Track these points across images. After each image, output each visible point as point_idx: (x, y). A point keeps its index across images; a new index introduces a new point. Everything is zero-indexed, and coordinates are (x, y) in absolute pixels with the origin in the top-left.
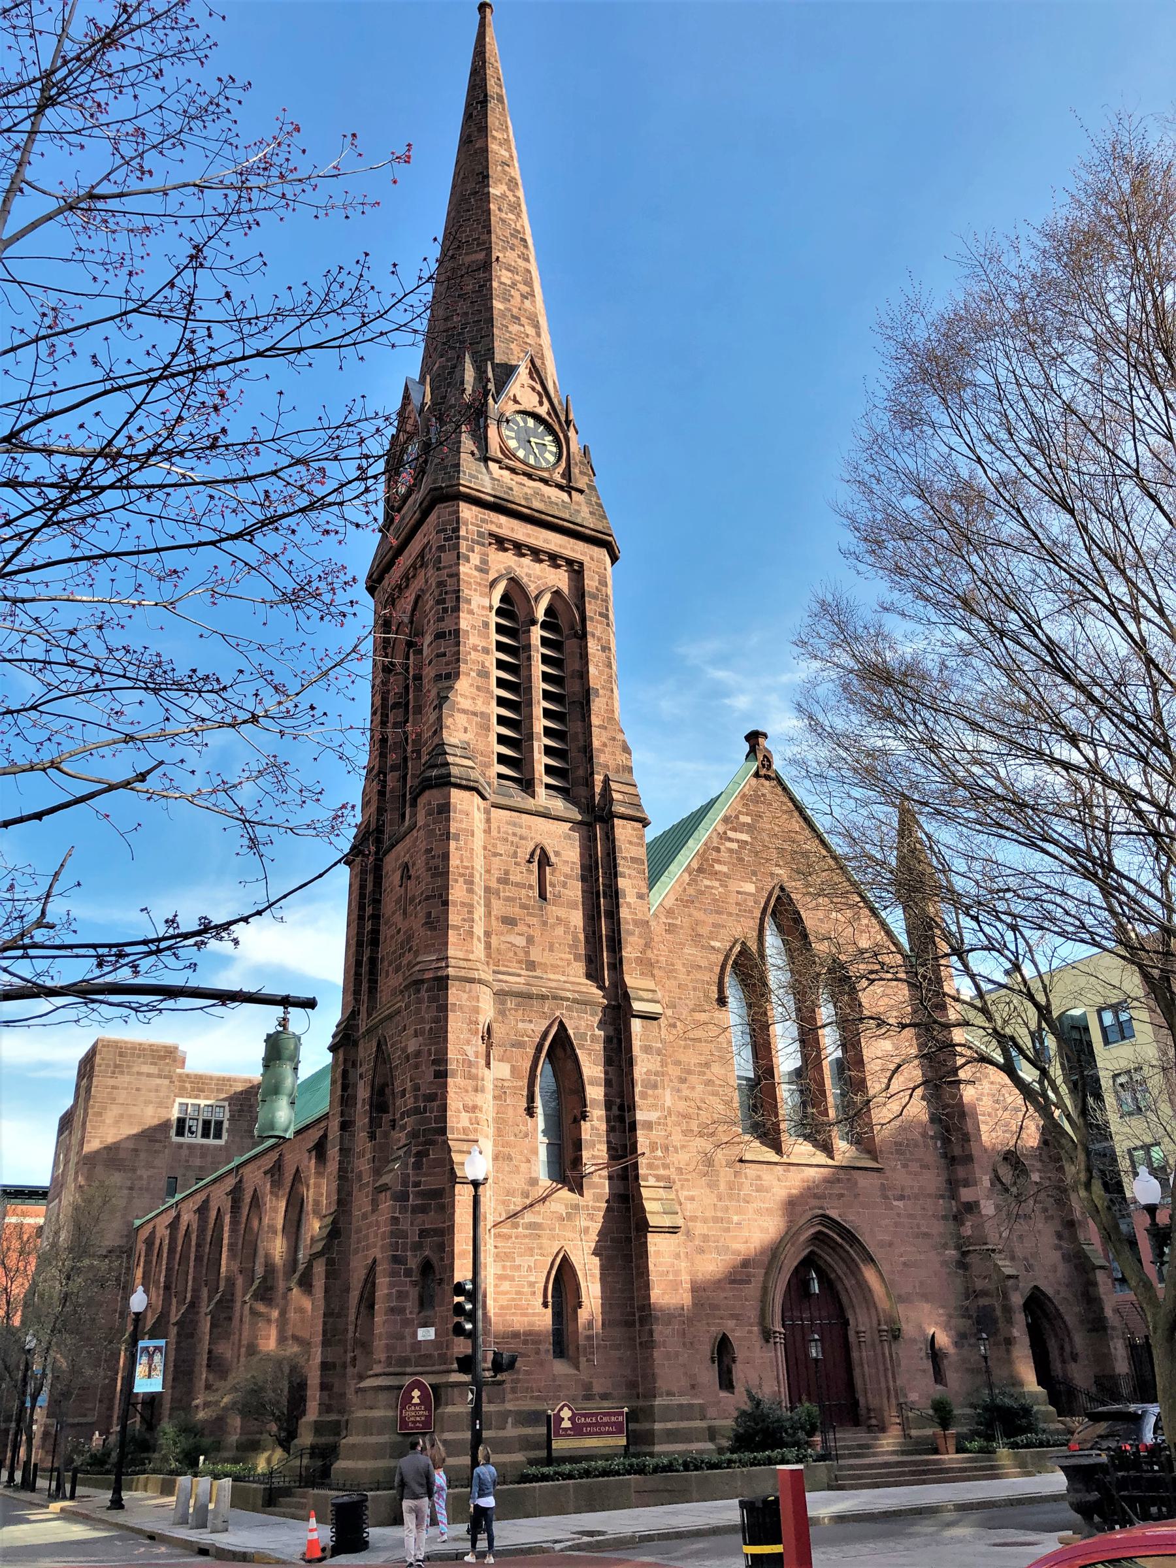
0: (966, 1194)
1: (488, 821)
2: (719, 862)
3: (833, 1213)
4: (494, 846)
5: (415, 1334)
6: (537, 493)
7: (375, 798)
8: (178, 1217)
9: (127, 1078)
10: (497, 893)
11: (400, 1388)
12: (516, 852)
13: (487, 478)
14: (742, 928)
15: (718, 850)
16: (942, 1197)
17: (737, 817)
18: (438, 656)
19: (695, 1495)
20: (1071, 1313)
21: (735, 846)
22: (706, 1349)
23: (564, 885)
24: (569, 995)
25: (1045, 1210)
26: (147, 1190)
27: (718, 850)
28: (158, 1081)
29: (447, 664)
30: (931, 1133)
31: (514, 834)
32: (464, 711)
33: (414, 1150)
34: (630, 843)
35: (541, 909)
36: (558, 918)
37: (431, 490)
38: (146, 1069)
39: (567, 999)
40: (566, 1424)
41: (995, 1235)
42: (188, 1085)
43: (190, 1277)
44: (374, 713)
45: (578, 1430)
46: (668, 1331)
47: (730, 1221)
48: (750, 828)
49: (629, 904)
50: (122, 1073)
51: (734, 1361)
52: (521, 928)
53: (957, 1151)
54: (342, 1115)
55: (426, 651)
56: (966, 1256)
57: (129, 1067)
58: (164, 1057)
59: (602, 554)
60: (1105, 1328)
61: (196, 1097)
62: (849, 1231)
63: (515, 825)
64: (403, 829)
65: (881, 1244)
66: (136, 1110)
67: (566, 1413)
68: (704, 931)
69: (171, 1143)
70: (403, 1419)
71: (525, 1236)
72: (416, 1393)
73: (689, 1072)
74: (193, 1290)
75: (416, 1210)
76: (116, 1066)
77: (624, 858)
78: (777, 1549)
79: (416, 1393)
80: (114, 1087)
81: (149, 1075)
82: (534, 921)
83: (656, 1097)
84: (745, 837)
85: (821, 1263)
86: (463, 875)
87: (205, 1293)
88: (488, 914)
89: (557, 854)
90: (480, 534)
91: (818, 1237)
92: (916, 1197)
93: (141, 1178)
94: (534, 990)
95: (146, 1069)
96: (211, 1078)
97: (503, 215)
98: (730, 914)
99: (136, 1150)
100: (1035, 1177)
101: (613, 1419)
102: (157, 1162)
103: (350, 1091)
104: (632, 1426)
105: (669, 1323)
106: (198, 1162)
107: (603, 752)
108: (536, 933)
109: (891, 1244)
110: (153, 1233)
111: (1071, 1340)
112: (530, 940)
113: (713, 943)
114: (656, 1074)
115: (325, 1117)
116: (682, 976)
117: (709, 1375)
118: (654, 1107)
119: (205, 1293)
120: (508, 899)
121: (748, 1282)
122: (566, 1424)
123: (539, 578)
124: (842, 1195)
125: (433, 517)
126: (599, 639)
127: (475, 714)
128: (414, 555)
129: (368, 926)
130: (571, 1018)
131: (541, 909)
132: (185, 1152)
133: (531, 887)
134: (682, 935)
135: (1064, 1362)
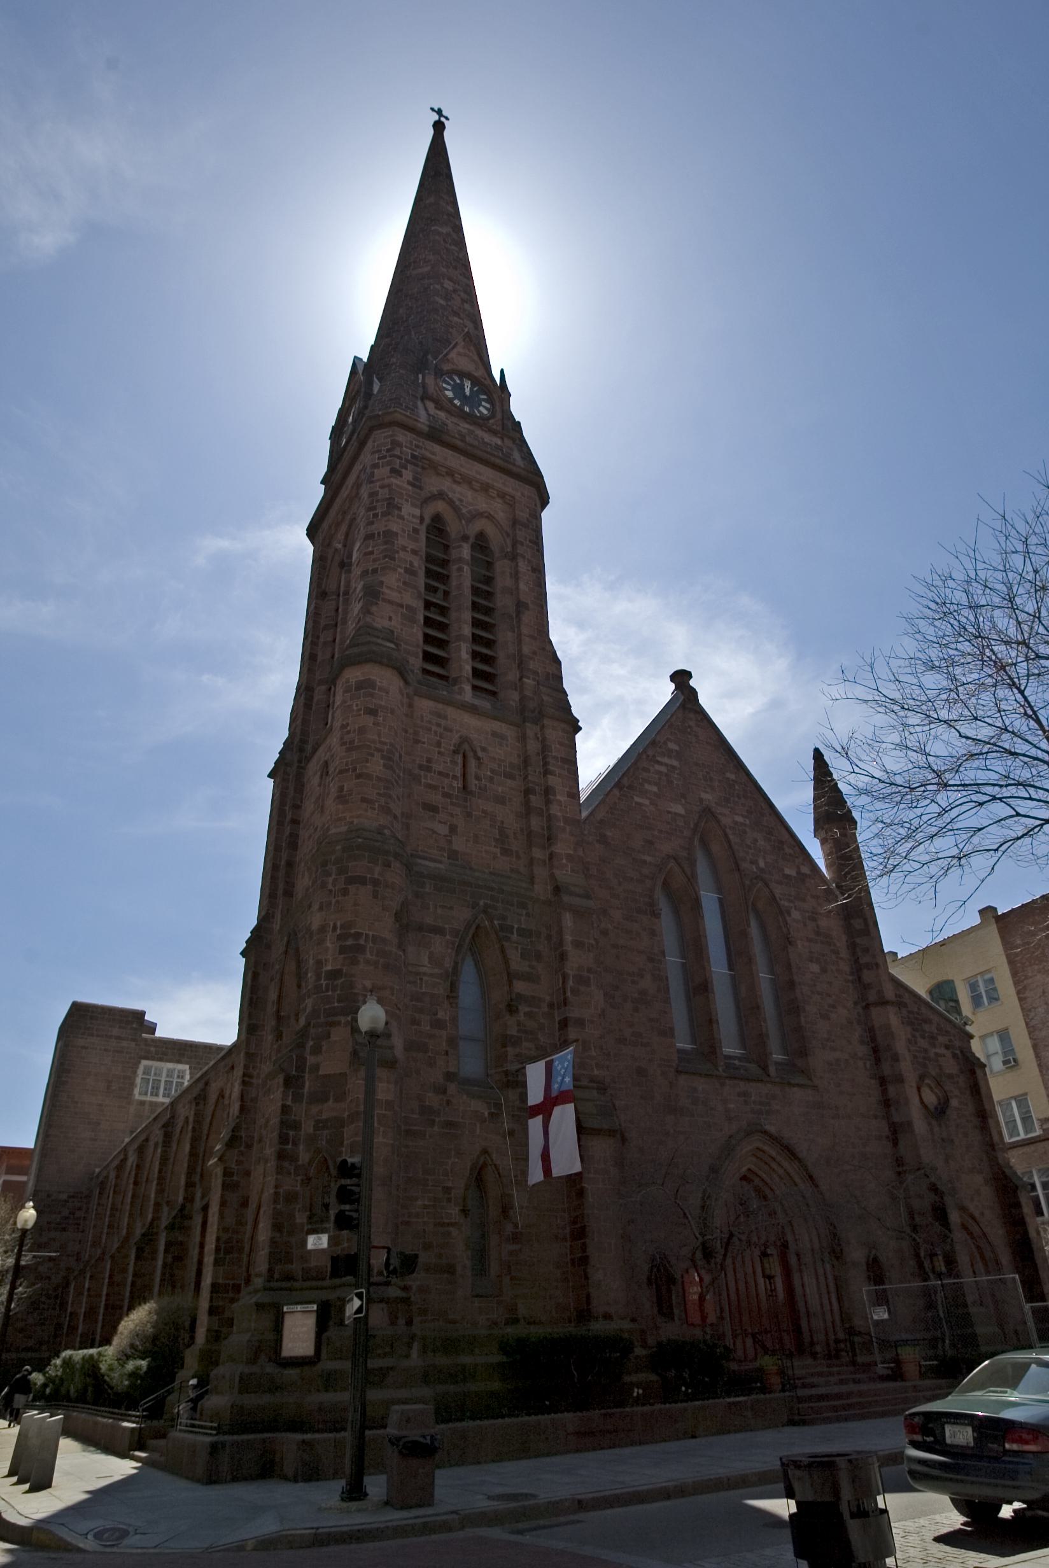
1: (410, 706)
6: (471, 432)
13: (422, 412)
16: (876, 1117)
17: (665, 743)
18: (366, 554)
21: (663, 769)
23: (491, 779)
29: (374, 560)
31: (439, 725)
32: (390, 602)
35: (466, 800)
36: (484, 811)
63: (439, 715)
77: (555, 758)
78: (24, 1178)
82: (458, 811)
84: (675, 763)
97: (448, 246)
112: (453, 829)
114: (589, 970)
120: (430, 786)
127: (401, 606)
131: (466, 800)
133: (455, 777)
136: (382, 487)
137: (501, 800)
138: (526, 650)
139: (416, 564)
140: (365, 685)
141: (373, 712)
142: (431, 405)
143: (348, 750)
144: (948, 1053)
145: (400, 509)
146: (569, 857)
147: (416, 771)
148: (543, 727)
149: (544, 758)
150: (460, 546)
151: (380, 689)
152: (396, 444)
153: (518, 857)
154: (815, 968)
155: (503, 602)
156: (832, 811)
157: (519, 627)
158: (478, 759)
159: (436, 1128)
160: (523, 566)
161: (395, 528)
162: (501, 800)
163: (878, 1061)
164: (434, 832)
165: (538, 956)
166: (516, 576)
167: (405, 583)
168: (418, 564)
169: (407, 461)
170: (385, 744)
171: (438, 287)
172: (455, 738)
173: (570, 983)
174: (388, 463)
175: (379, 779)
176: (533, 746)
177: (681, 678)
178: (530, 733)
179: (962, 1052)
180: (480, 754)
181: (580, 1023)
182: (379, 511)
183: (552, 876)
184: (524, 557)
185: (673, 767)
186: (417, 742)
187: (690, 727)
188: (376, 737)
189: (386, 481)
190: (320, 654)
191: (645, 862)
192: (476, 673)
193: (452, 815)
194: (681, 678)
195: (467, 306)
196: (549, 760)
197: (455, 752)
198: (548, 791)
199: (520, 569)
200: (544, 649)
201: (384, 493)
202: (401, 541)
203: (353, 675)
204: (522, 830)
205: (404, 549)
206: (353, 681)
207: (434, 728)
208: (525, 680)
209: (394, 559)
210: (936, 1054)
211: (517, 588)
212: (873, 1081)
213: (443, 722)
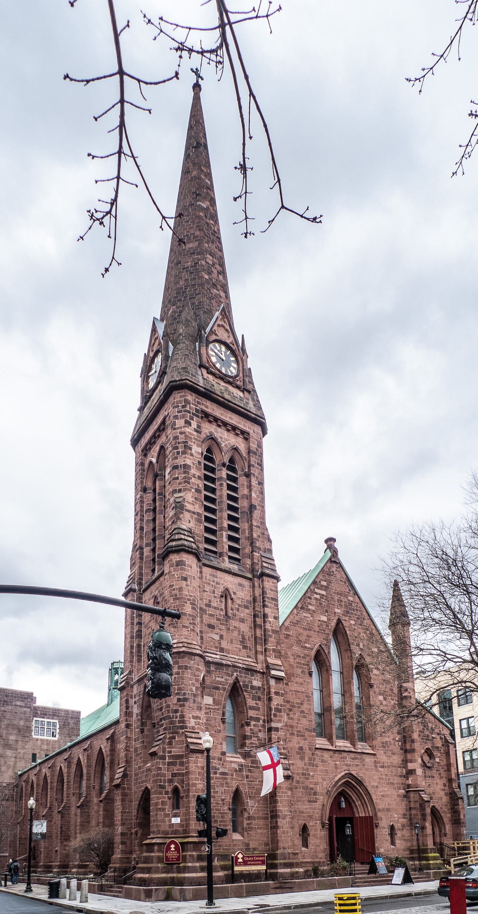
0: (410, 766)
1: (201, 572)
2: (310, 604)
3: (354, 773)
4: (204, 587)
5: (170, 820)
7: (138, 561)
8: (40, 770)
9: (10, 707)
10: (205, 611)
11: (165, 843)
12: (214, 591)
14: (316, 642)
15: (310, 598)
16: (400, 767)
17: (320, 582)
19: (169, 879)
20: (446, 817)
21: (318, 597)
22: (297, 829)
23: (238, 610)
24: (240, 665)
25: (440, 774)
26: (23, 758)
27: (310, 598)
28: (25, 709)
29: (180, 484)
30: (397, 739)
31: (214, 581)
33: (168, 736)
34: (271, 590)
36: (235, 627)
37: (171, 382)
38: (18, 703)
39: (239, 667)
40: (240, 860)
41: (422, 783)
42: (39, 712)
43: (49, 796)
44: (136, 515)
45: (245, 863)
46: (284, 822)
47: (309, 775)
48: (326, 588)
49: (270, 622)
50: (8, 705)
51: (309, 836)
52: (217, 630)
53: (408, 747)
54: (126, 720)
55: (167, 477)
56: (409, 791)
57: (11, 702)
58: (27, 698)
59: (258, 429)
60: (459, 823)
61: (43, 718)
62: (360, 781)
63: (214, 576)
64: (154, 578)
65: (373, 787)
66: (15, 722)
67: (240, 856)
68: (303, 638)
69: (33, 739)
70: (167, 857)
71: (220, 778)
72: (173, 846)
73: (294, 706)
74: (50, 802)
75: (169, 764)
76: (5, 701)
77: (268, 598)
79: (173, 846)
80: (4, 711)
81: (20, 706)
82: (223, 627)
83: (281, 716)
85: (345, 794)
86: (189, 600)
87: (94, 793)
88: (202, 621)
89: (234, 593)
90: (197, 410)
91: (347, 783)
92: (389, 767)
93: (20, 753)
94: (224, 662)
95: (18, 703)
96: (49, 709)
98: (315, 631)
99: (17, 741)
100: (437, 760)
101: (260, 858)
102: (27, 747)
103: (130, 710)
104: (269, 862)
105: (284, 818)
106: (45, 747)
107: (258, 540)
108: (224, 633)
109: (377, 787)
110: (28, 777)
111: (445, 828)
112: (221, 637)
113: (306, 645)
115: (117, 722)
116: (291, 660)
117: (298, 841)
118: (280, 721)
119: (94, 793)
120: (211, 615)
121: (316, 802)
122: (240, 860)
123: (226, 440)
124: (357, 765)
125: (171, 399)
126: (257, 478)
127: (194, 513)
128: (159, 423)
129: (136, 628)
130: (241, 677)
132: (39, 743)
134: (293, 640)
135: (440, 836)
136: (181, 433)
137: (242, 620)
138: (255, 535)
139: (200, 486)
140: (180, 563)
141: (185, 579)
142: (204, 371)
143: (174, 599)
144: (438, 737)
145: (191, 449)
146: (274, 650)
147: (204, 607)
148: (263, 581)
149: (263, 598)
150: (221, 470)
151: (189, 566)
152: (187, 402)
153: (250, 650)
154: (381, 698)
155: (243, 504)
156: (399, 619)
157: (251, 521)
158: (232, 599)
159: (218, 775)
160: (254, 482)
161: (188, 462)
162: (242, 620)
163: (405, 742)
164: (214, 639)
165: (259, 699)
166: (250, 487)
167: (196, 498)
168: (201, 484)
169: (193, 414)
170: (191, 596)
171: (204, 263)
172: (222, 589)
173: (273, 712)
174: (183, 416)
175: (190, 615)
176: (258, 592)
177: (330, 542)
178: (256, 584)
179: (445, 737)
180: (233, 596)
181: (277, 729)
182: (180, 450)
183: (266, 661)
184: (254, 475)
185: (323, 595)
186: (204, 591)
187: (333, 572)
188: (187, 593)
189: (183, 429)
190: (145, 527)
191: (306, 647)
192: (231, 549)
193: (221, 630)
194: (330, 542)
195: (221, 277)
196: (266, 599)
197: (222, 596)
198: (265, 616)
199: (253, 484)
200: (263, 534)
201: (182, 438)
202: (193, 471)
203: (174, 558)
204: (252, 636)
205: (194, 476)
206: (174, 561)
207: (211, 583)
208: (254, 553)
209: (189, 483)
210: (433, 738)
211: (251, 495)
212: (401, 751)
213: (215, 579)
